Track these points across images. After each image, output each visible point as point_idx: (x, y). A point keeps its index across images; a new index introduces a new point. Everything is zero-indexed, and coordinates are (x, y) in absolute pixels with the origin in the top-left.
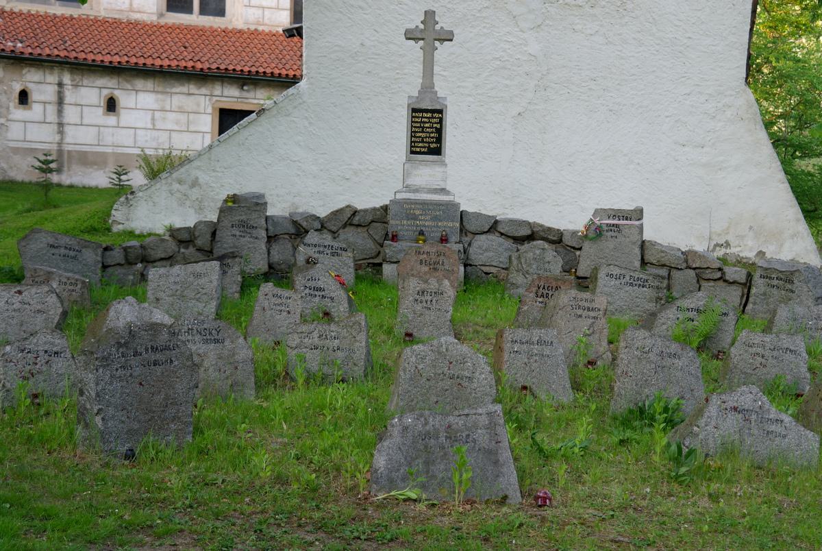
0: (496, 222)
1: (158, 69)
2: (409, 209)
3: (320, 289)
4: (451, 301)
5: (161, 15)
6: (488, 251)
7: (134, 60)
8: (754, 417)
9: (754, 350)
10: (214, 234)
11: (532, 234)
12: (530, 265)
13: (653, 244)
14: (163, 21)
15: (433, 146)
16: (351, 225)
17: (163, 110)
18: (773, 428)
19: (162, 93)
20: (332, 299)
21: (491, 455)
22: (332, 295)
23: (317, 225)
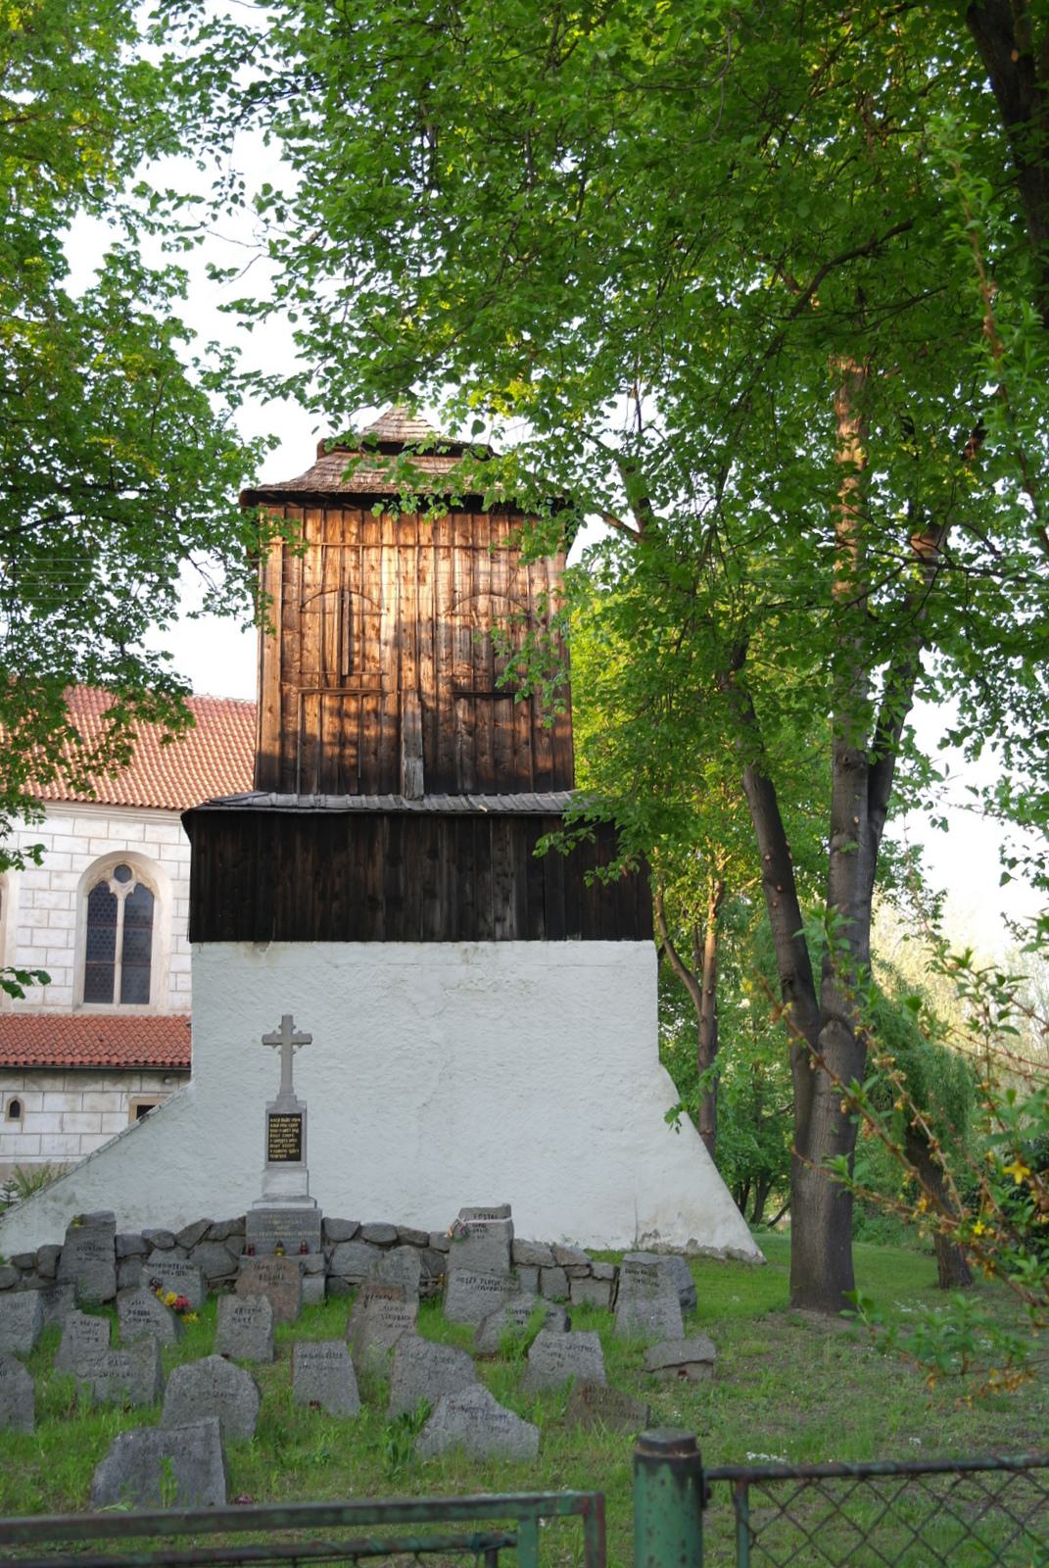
0: (360, 1228)
1: (68, 1066)
2: (265, 1219)
3: (145, 1313)
4: (269, 1318)
5: (77, 1007)
6: (350, 1259)
7: (42, 1058)
8: (480, 1414)
9: (552, 1350)
10: (58, 1258)
11: (395, 1240)
12: (387, 1273)
13: (522, 1242)
14: (78, 1014)
15: (292, 1151)
16: (207, 1240)
17: (73, 1112)
18: (497, 1423)
19: (73, 1092)
20: (157, 1322)
21: (204, 1465)
22: (158, 1318)
23: (170, 1242)
